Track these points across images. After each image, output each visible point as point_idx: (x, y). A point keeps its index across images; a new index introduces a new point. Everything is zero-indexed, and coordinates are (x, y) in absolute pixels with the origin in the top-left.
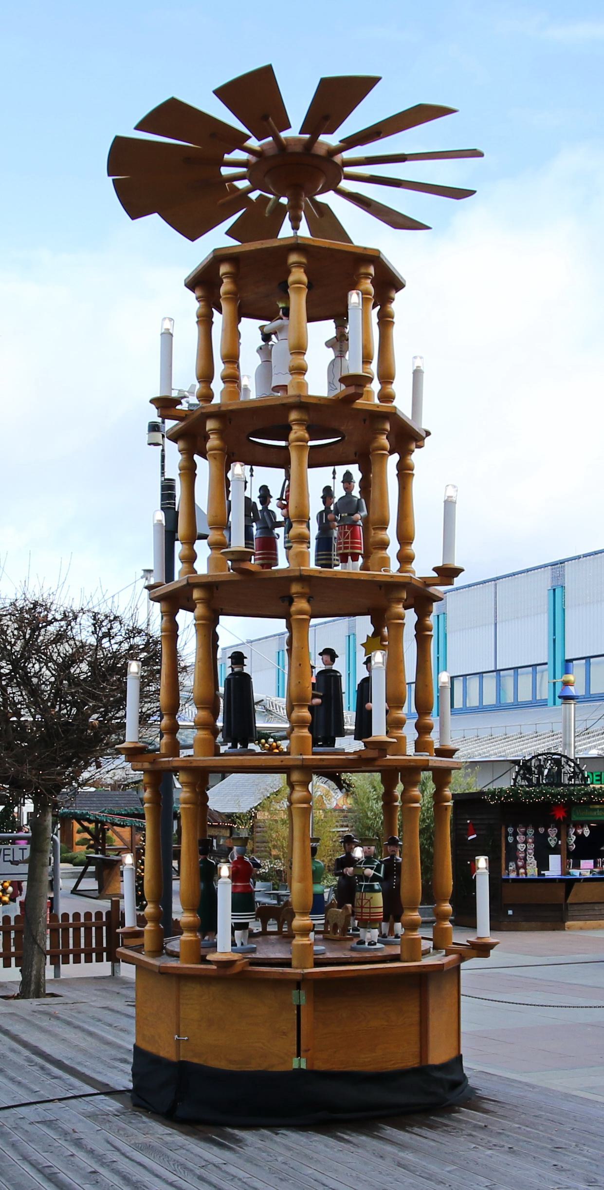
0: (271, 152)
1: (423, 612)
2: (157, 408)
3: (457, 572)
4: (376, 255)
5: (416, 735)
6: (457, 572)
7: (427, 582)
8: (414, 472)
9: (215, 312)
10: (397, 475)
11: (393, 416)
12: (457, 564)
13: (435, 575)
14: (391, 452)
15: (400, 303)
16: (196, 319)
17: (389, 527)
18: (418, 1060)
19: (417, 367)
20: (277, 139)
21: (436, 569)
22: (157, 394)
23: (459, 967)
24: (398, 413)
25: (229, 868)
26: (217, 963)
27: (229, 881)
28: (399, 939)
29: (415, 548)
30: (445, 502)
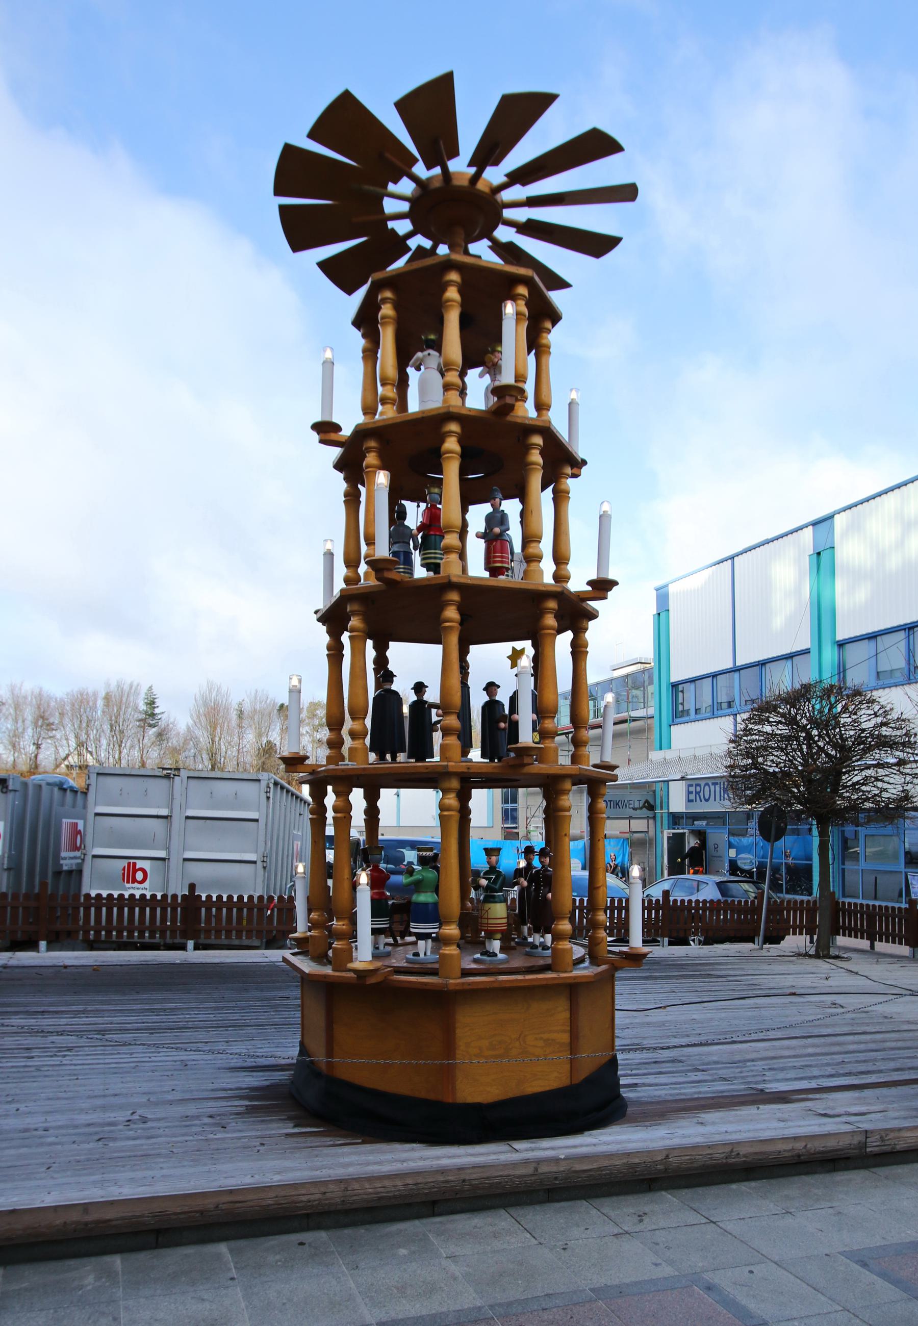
0: (437, 184)
1: (579, 631)
2: (318, 434)
3: (612, 584)
4: (547, 425)
5: (554, 568)
6: (612, 584)
7: (582, 597)
8: (588, 649)
9: (360, 486)
10: (571, 653)
11: (548, 433)
12: (611, 576)
13: (590, 588)
14: (560, 631)
15: (555, 337)
16: (361, 355)
17: (528, 382)
18: (569, 1079)
19: (572, 399)
20: (445, 169)
21: (590, 583)
22: (318, 418)
23: (613, 976)
24: (552, 428)
25: (367, 875)
26: (355, 971)
27: (368, 888)
28: (550, 951)
29: (572, 568)
30: (601, 516)
